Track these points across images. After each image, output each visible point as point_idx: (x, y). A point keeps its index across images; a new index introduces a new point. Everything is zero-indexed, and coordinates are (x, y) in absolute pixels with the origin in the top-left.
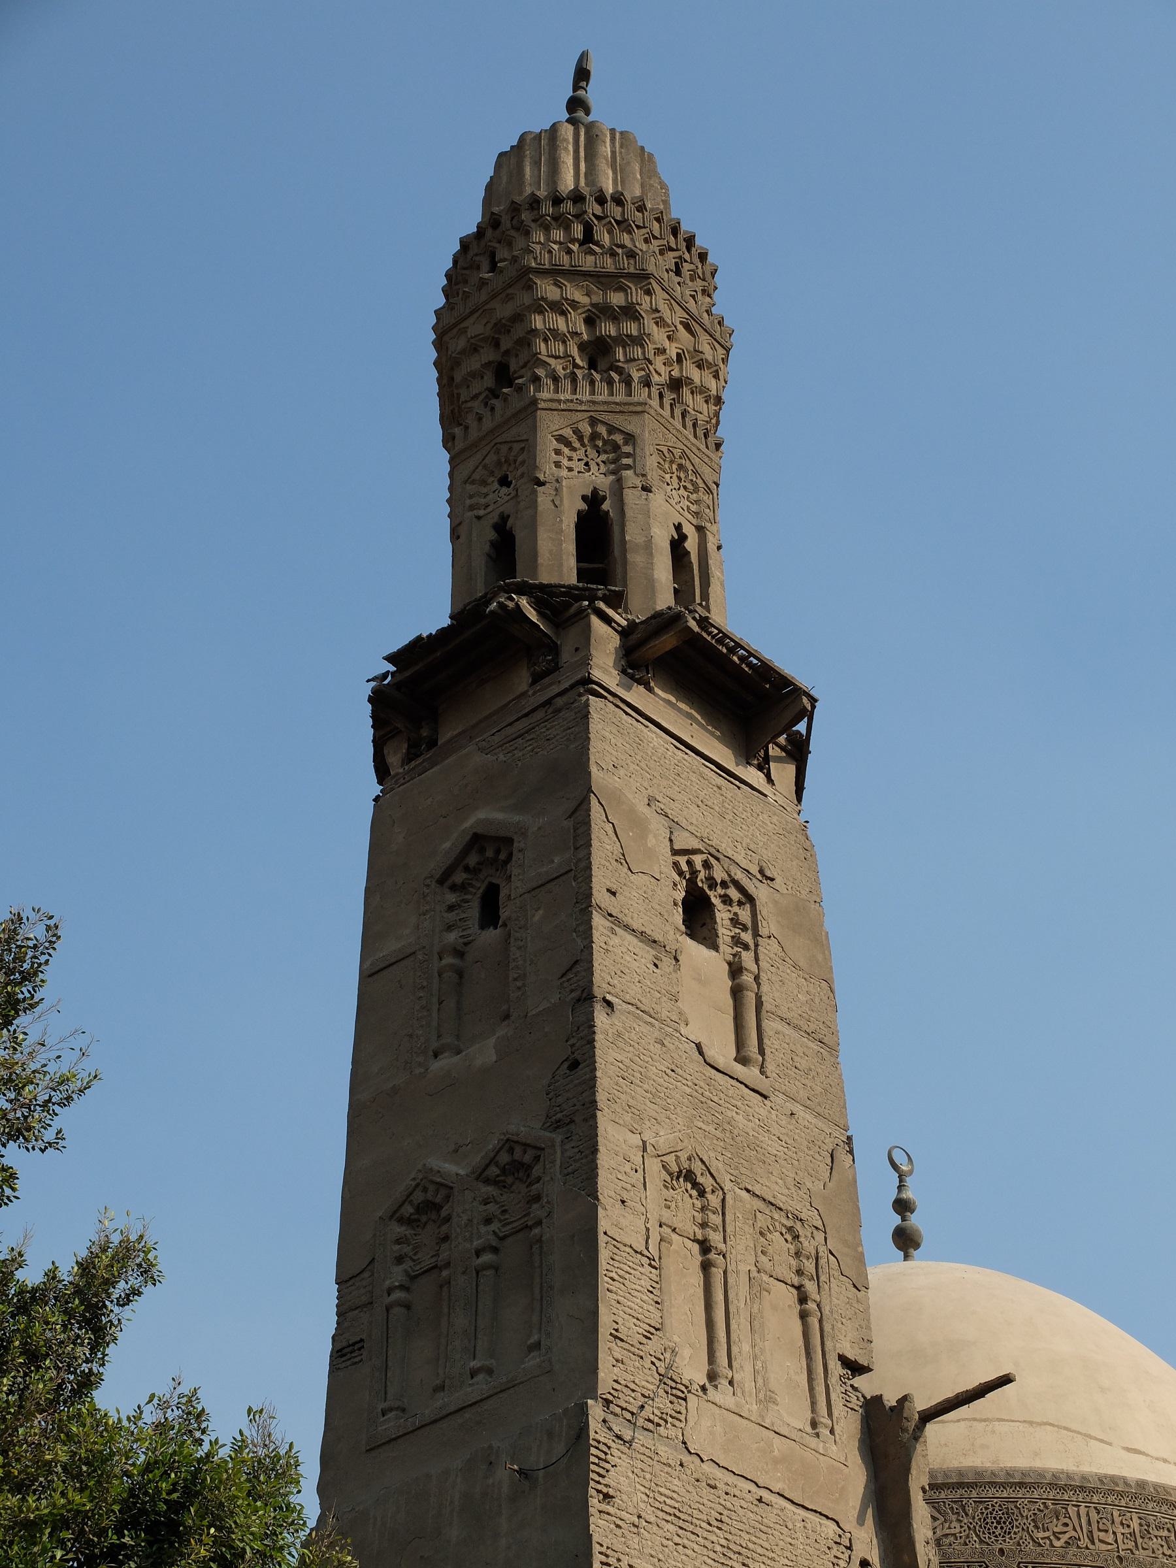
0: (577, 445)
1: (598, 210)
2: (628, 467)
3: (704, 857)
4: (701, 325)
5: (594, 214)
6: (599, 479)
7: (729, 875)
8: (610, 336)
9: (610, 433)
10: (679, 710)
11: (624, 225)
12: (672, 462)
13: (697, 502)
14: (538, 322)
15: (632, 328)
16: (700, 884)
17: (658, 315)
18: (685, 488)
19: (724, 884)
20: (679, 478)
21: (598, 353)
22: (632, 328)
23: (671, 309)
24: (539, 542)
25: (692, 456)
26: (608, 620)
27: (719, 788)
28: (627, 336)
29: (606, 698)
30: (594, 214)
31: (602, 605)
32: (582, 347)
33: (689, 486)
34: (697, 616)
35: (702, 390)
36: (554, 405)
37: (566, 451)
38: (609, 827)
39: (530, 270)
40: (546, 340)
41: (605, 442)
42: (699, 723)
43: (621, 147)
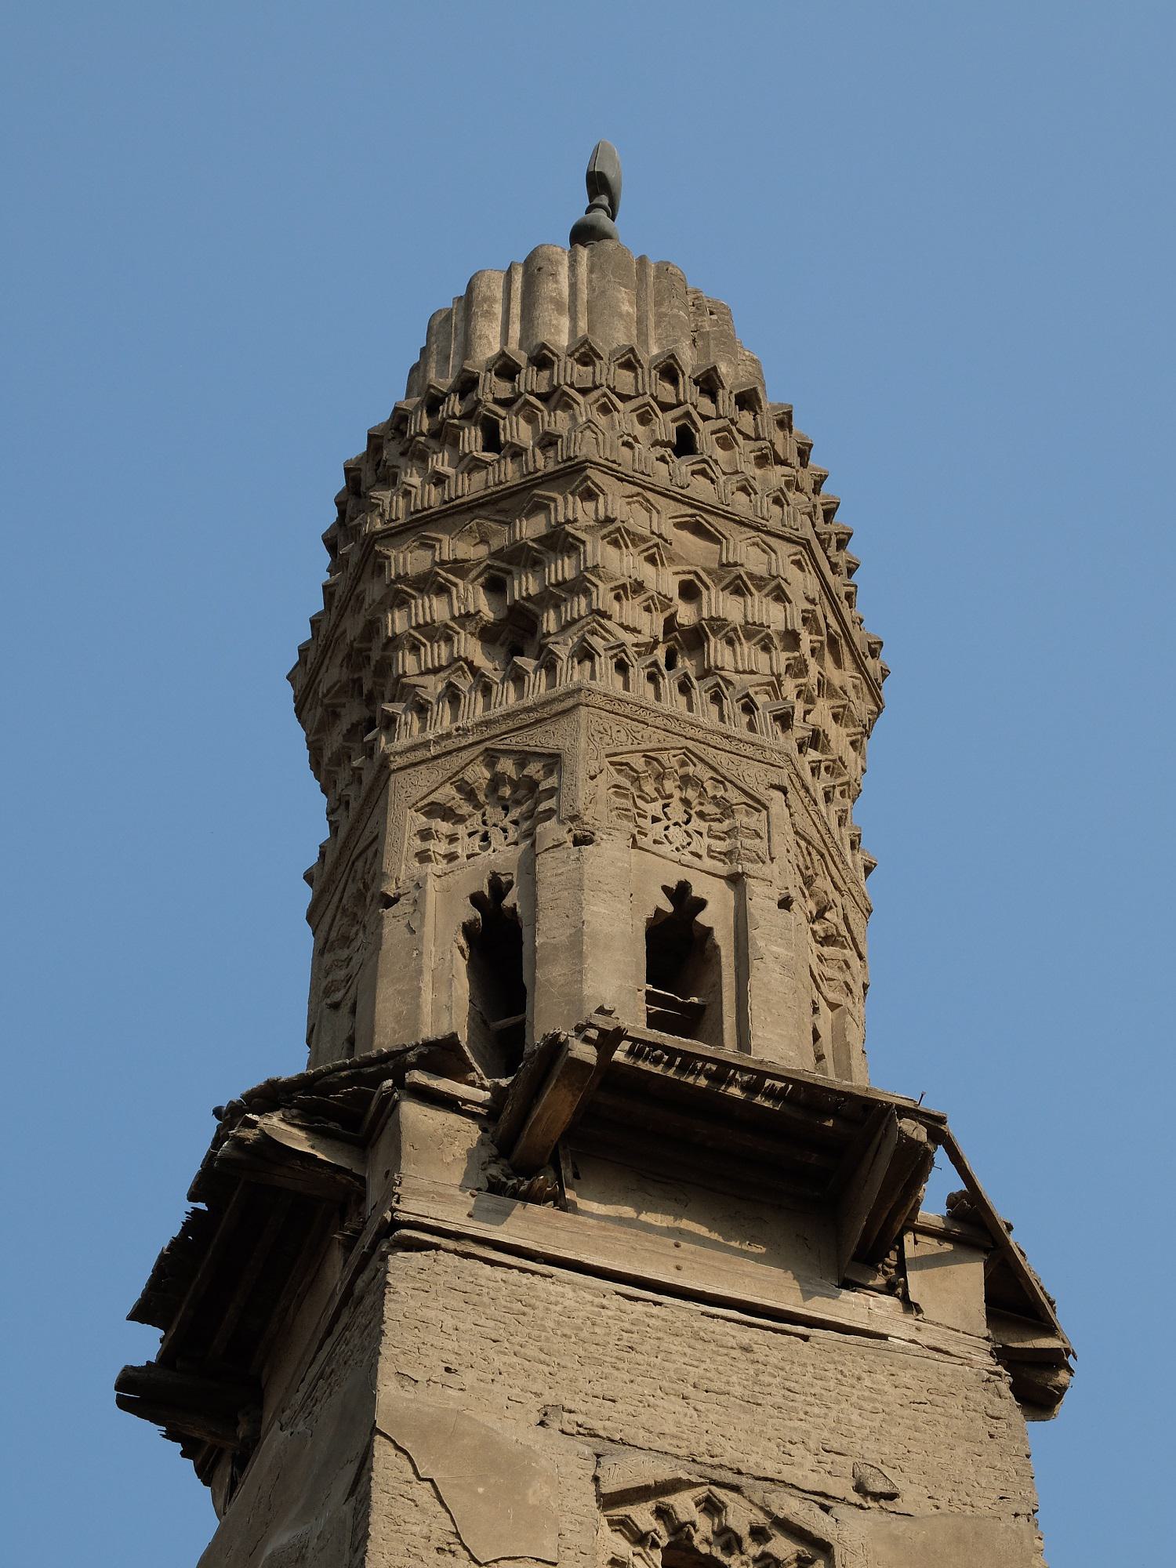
0: (466, 809)
1: (504, 389)
2: (549, 814)
3: (701, 1492)
4: (727, 516)
5: (496, 401)
6: (503, 855)
7: (769, 1514)
8: (529, 598)
9: (521, 765)
10: (648, 1228)
11: (554, 398)
12: (660, 777)
13: (730, 833)
14: (397, 622)
15: (564, 568)
16: (704, 1549)
17: (611, 528)
18: (701, 815)
19: (759, 1534)
20: (686, 802)
21: (516, 634)
22: (564, 568)
23: (649, 507)
24: (379, 1007)
25: (709, 754)
26: (449, 1103)
27: (746, 1349)
28: (558, 585)
29: (437, 1247)
30: (496, 401)
31: (418, 1077)
32: (488, 635)
33: (710, 809)
34: (593, 1034)
35: (754, 632)
36: (420, 755)
37: (444, 827)
38: (423, 1493)
39: (375, 537)
40: (415, 648)
41: (516, 785)
42: (714, 1245)
43: (591, 271)
